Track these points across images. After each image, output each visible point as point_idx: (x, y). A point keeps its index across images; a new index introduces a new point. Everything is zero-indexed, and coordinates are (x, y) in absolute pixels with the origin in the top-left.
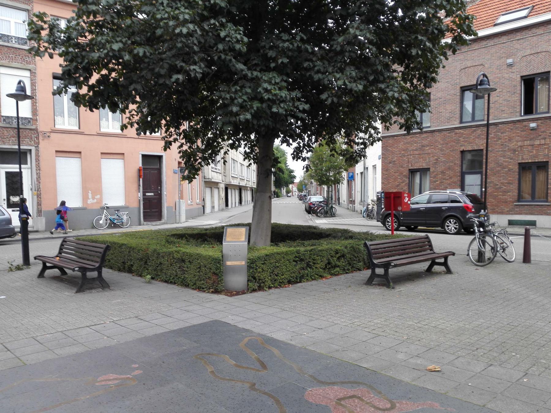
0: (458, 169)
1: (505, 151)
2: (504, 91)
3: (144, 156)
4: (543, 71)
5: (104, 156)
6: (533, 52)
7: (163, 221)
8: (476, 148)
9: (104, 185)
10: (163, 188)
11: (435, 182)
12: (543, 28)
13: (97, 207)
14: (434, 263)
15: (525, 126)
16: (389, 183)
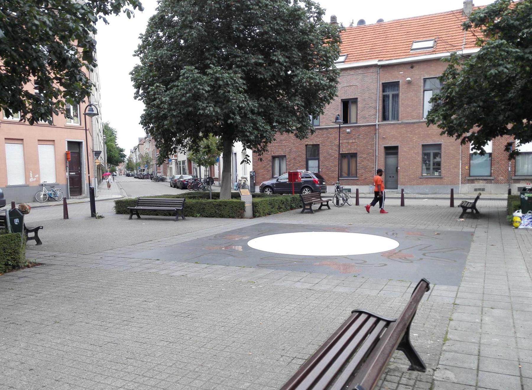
0: (304, 156)
1: (332, 146)
2: (331, 108)
3: (69, 142)
4: (354, 97)
5: (41, 142)
6: (348, 85)
7: (83, 195)
8: (315, 143)
9: (41, 166)
10: (82, 169)
11: (290, 165)
12: (353, 71)
13: (36, 184)
14: (322, 205)
15: (344, 131)
16: (258, 165)
